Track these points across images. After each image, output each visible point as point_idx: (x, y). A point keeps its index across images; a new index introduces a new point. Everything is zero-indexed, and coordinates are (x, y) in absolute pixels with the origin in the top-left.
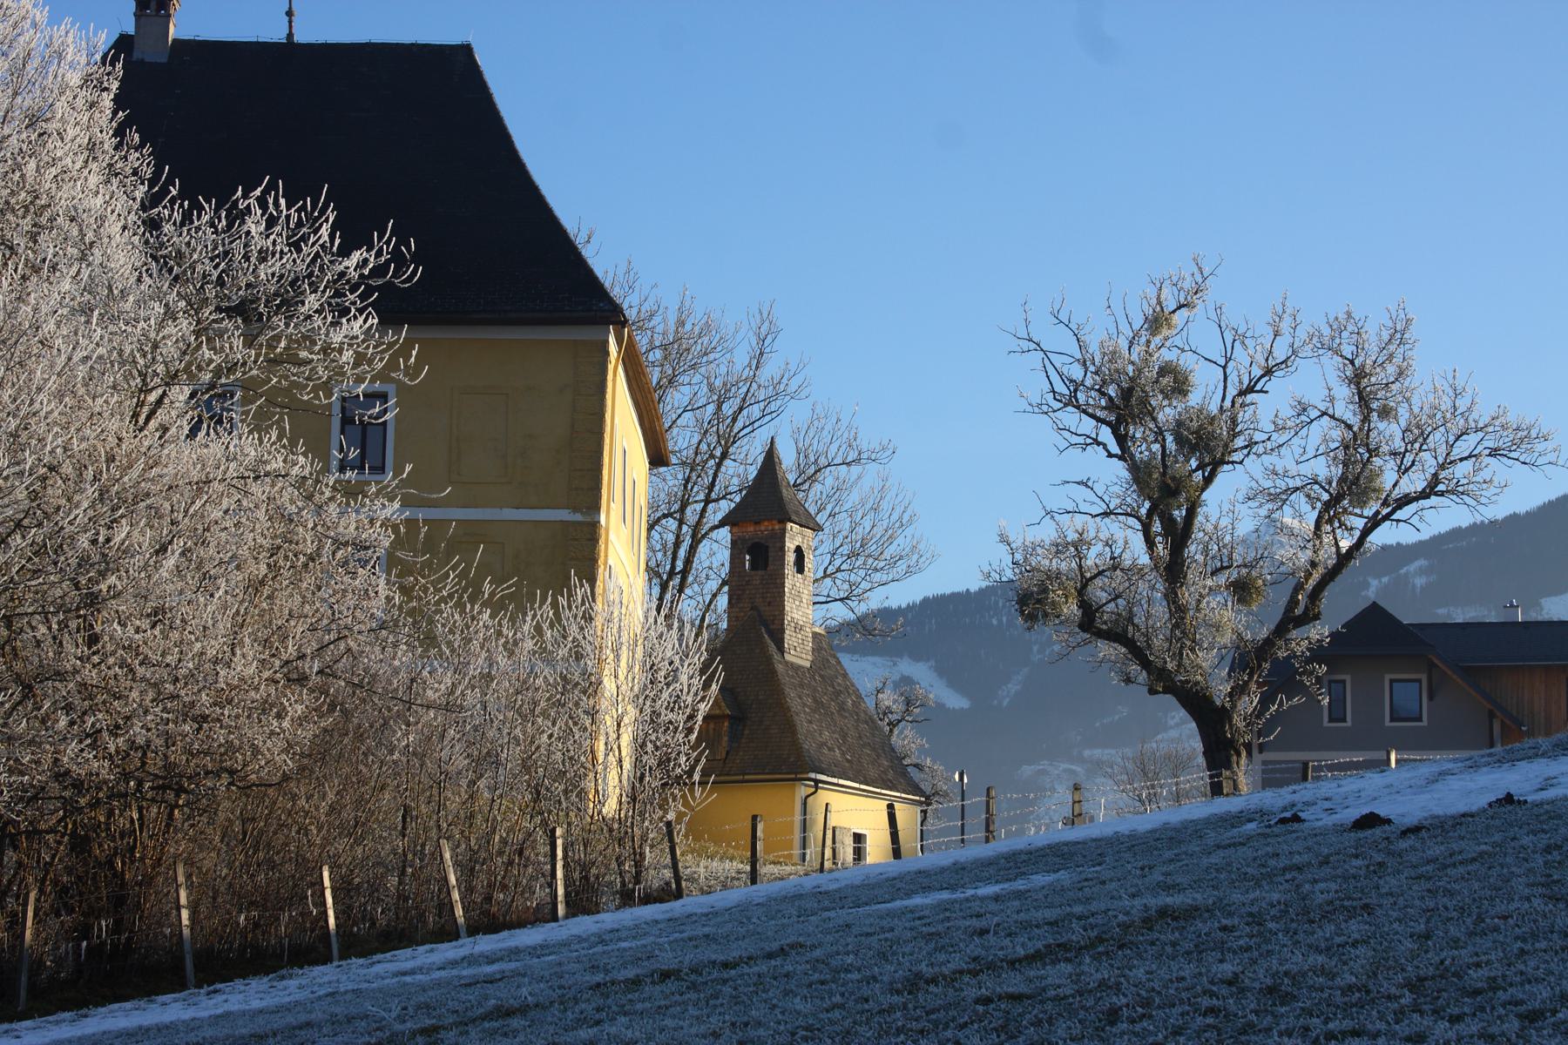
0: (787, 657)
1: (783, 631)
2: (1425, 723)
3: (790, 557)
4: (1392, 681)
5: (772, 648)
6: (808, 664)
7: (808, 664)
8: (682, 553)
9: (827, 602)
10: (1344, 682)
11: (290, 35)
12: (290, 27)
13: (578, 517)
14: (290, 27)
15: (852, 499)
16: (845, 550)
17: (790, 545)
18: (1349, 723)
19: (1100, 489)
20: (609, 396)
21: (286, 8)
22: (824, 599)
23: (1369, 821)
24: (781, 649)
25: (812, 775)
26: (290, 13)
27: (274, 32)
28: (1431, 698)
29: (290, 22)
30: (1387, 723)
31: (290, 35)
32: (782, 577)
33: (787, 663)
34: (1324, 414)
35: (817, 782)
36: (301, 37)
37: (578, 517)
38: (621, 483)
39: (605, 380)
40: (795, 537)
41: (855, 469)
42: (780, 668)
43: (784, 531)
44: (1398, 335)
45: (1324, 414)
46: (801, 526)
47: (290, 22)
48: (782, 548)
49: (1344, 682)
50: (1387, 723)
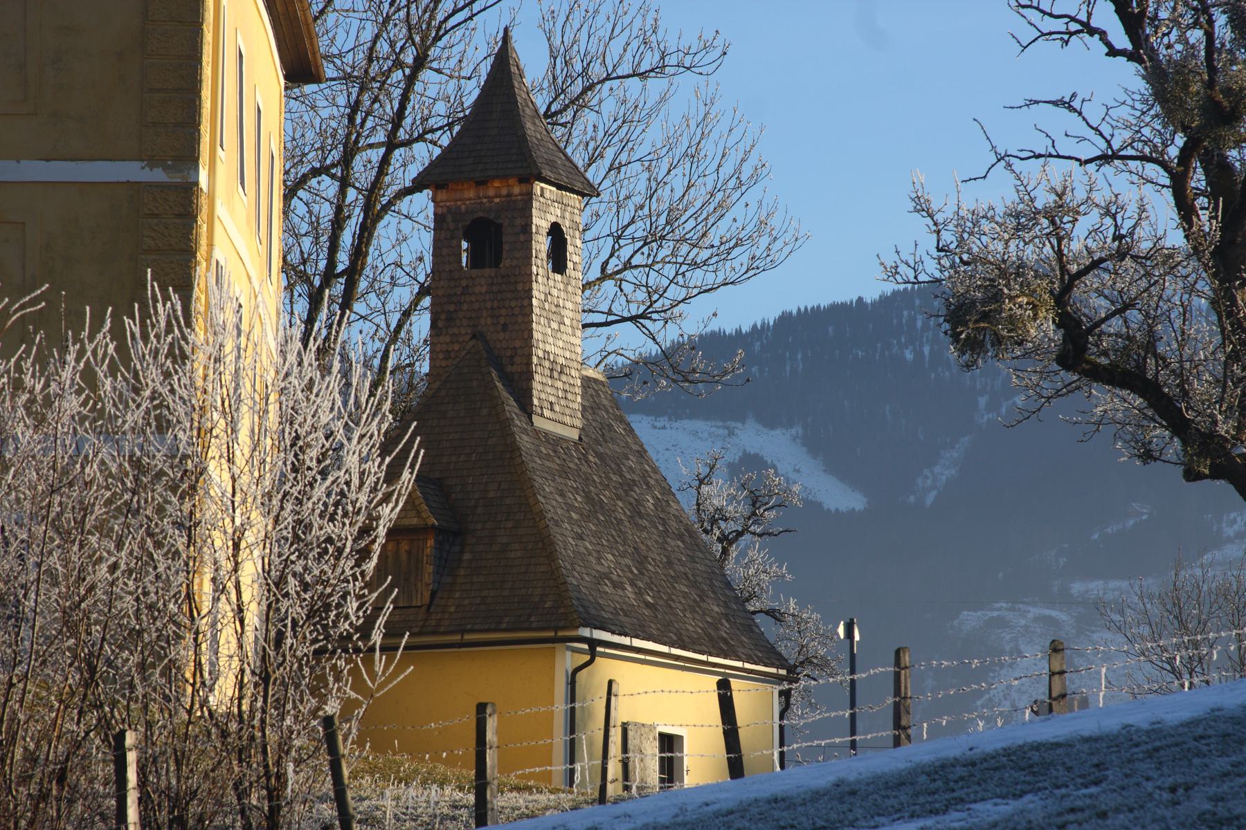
0: (538, 422)
1: (530, 378)
3: (541, 245)
5: (511, 406)
6: (574, 435)
7: (574, 435)
8: (347, 238)
13: (158, 175)
15: (651, 138)
16: (639, 229)
17: (541, 222)
22: (601, 318)
25: (585, 632)
32: (528, 279)
37: (158, 175)
41: (655, 85)
42: (525, 441)
43: (528, 197)
48: (526, 229)
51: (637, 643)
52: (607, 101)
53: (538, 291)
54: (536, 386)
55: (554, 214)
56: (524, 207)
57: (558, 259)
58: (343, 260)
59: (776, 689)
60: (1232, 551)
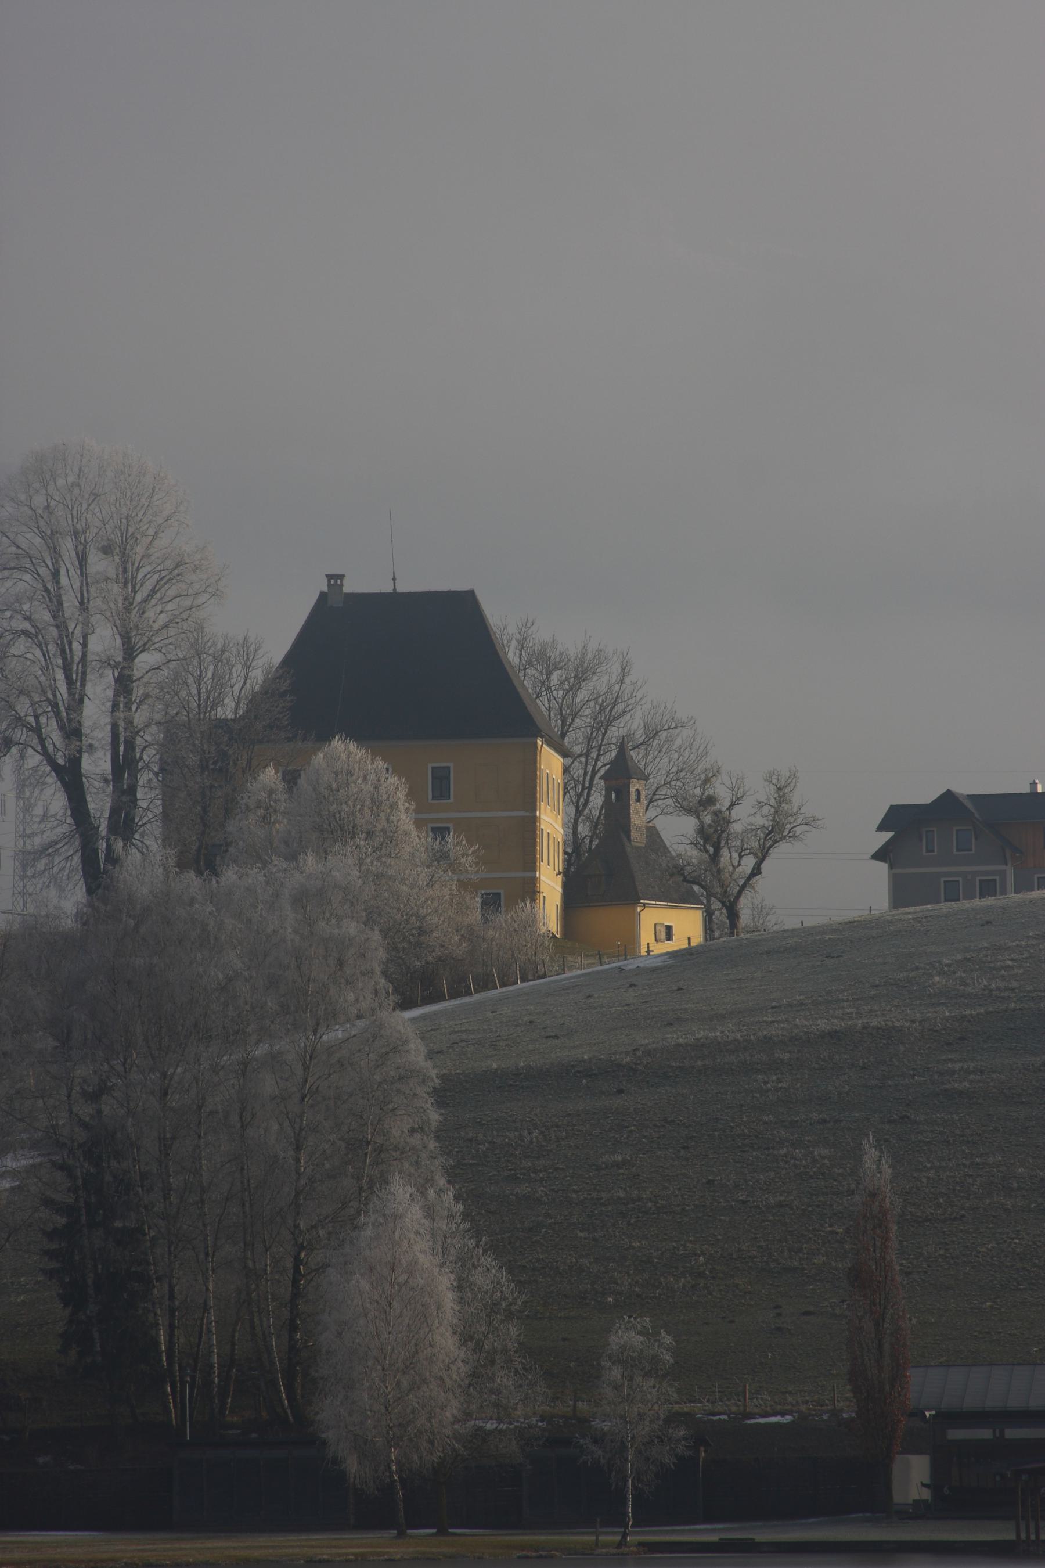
0: (633, 844)
1: (630, 831)
2: (936, 853)
3: (633, 796)
4: (957, 831)
5: (625, 839)
6: (644, 845)
7: (644, 845)
8: (588, 778)
9: (664, 799)
10: (933, 831)
11: (395, 589)
12: (395, 586)
13: (528, 814)
14: (395, 586)
15: (678, 743)
16: (675, 769)
17: (633, 790)
18: (973, 852)
19: (688, 836)
20: (538, 758)
21: (392, 577)
22: (663, 797)
23: (638, 967)
24: (629, 840)
25: (642, 901)
26: (394, 579)
27: (389, 589)
28: (976, 839)
29: (394, 583)
30: (955, 852)
31: (395, 589)
32: (629, 805)
33: (632, 846)
34: (766, 804)
35: (644, 904)
36: (400, 589)
37: (528, 814)
38: (552, 788)
39: (536, 758)
40: (634, 786)
41: (677, 731)
42: (628, 849)
43: (629, 783)
44: (794, 775)
45: (766, 804)
46: (638, 779)
47: (394, 583)
48: (629, 792)
49: (933, 831)
50: (955, 852)
51: (657, 903)
52: (663, 735)
53: (632, 808)
54: (632, 834)
55: (637, 786)
56: (627, 787)
57: (638, 800)
58: (587, 784)
59: (701, 911)
60: (10, 1162)
